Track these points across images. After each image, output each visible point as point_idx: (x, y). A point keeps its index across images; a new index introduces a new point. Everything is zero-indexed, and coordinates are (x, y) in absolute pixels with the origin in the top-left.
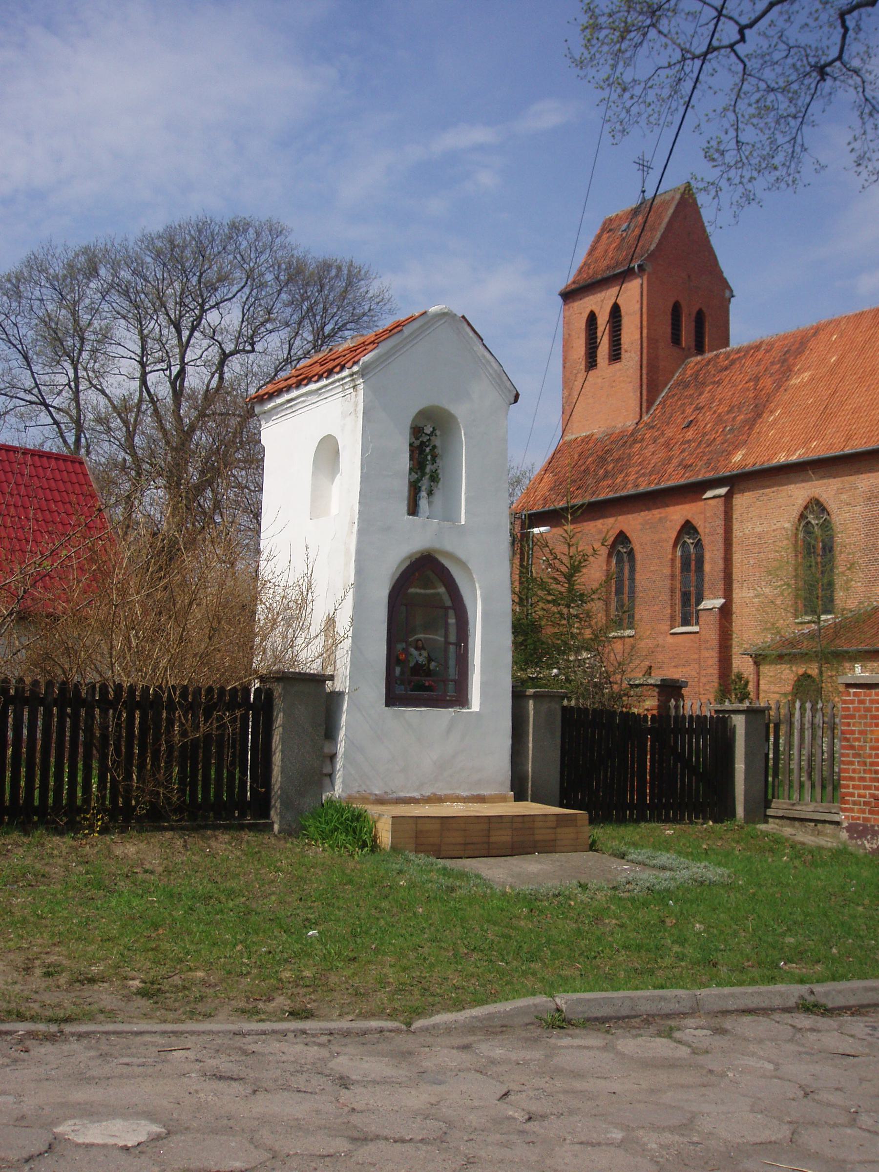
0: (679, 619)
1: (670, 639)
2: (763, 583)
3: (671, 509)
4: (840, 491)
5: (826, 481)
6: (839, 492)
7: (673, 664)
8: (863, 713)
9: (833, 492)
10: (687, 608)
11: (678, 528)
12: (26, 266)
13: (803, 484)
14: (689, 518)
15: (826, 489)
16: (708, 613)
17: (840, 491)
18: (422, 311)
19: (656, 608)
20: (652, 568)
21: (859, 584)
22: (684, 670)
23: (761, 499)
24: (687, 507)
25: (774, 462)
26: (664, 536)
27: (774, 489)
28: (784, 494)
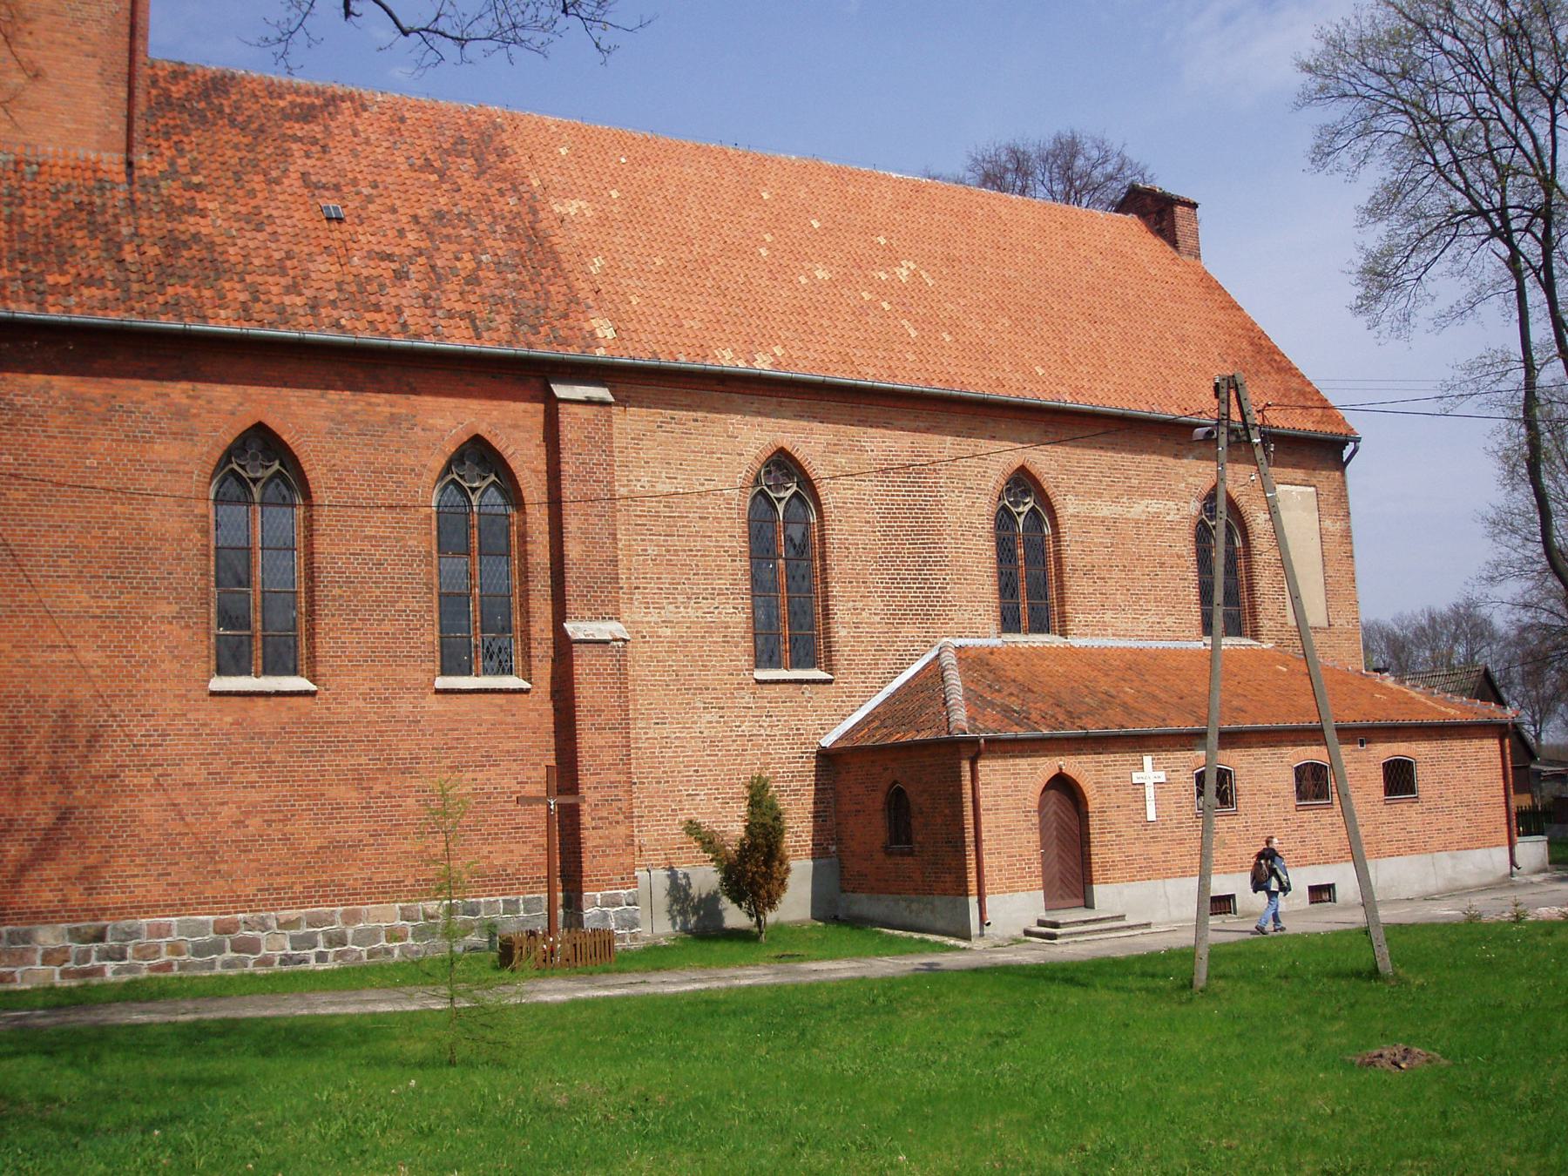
0: (1218, 623)
1: (434, 704)
2: (680, 598)
3: (427, 402)
4: (831, 448)
5: (803, 423)
6: (832, 449)
7: (448, 762)
8: (383, 943)
9: (820, 448)
10: (474, 631)
11: (451, 449)
12: (1324, 166)
13: (764, 420)
14: (482, 430)
15: (811, 441)
16: (598, 649)
17: (831, 448)
18: (1193, 199)
19: (387, 627)
20: (369, 531)
21: (877, 619)
22: (480, 776)
23: (667, 427)
24: (475, 405)
25: (710, 364)
26: (409, 461)
27: (700, 415)
28: (717, 429)
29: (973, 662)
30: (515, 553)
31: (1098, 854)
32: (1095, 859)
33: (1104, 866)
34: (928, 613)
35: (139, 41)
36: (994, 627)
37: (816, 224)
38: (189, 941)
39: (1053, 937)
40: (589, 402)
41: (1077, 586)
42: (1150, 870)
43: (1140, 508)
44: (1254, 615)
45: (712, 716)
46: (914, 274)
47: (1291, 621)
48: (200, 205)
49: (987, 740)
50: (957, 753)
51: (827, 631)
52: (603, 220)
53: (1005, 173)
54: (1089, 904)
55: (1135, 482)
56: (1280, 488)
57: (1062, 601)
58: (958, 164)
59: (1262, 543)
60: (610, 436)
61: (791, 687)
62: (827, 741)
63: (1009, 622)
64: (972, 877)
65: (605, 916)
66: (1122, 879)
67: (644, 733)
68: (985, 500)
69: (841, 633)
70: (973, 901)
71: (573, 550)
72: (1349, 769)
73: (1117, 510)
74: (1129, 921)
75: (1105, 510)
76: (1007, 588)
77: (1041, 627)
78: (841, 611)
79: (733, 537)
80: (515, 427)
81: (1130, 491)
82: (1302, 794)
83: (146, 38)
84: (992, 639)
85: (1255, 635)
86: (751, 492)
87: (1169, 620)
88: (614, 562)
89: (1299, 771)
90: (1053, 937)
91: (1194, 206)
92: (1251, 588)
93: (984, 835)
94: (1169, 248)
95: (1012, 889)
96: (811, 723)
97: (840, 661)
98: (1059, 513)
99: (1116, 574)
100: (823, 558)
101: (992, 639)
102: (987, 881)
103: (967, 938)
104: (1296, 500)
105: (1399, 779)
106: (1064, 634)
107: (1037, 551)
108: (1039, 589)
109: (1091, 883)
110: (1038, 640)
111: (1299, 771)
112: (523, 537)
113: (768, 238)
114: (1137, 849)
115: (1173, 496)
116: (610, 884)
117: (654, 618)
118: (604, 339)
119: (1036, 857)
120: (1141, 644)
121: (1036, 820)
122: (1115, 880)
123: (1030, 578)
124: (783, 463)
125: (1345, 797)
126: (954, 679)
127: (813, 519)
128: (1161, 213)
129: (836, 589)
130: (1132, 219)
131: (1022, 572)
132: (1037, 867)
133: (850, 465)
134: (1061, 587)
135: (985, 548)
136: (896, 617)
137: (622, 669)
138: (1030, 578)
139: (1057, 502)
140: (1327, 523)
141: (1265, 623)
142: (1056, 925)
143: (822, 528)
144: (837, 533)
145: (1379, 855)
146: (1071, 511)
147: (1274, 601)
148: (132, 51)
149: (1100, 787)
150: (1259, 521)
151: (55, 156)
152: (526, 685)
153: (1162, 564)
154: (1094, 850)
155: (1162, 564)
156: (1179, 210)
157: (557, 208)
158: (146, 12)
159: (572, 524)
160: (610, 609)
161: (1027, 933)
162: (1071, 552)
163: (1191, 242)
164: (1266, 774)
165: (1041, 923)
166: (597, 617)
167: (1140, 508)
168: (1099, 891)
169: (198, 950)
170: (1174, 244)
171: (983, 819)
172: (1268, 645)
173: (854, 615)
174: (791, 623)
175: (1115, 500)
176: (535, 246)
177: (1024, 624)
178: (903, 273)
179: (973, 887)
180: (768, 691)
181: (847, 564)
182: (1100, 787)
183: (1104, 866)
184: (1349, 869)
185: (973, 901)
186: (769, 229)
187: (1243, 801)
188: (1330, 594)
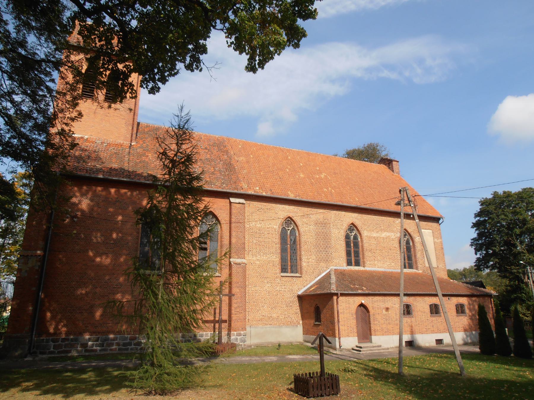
29: (341, 274)
30: (219, 241)
31: (374, 327)
32: (372, 328)
33: (375, 330)
34: (327, 260)
35: (135, 116)
36: (345, 264)
37: (301, 164)
38: (122, 342)
39: (360, 351)
40: (239, 203)
41: (367, 254)
42: (388, 332)
43: (384, 234)
44: (416, 263)
45: (269, 285)
46: (325, 176)
47: (427, 265)
48: (147, 154)
49: (341, 294)
50: (329, 297)
51: (301, 263)
52: (248, 162)
53: (353, 155)
54: (371, 342)
55: (382, 228)
56: (423, 230)
57: (363, 259)
58: (342, 152)
59: (418, 246)
60: (245, 212)
61: (290, 278)
62: (300, 293)
63: (349, 263)
64: (337, 332)
65: (237, 339)
66: (380, 335)
67: (250, 289)
68: (342, 231)
69: (304, 264)
70: (337, 339)
71: (234, 240)
72: (446, 306)
73: (378, 235)
74: (382, 347)
75: (375, 235)
76: (348, 254)
77: (357, 264)
78: (304, 258)
79: (277, 239)
80: (221, 209)
81: (381, 230)
82: (431, 313)
83: (137, 116)
84: (344, 267)
85: (417, 269)
86: (281, 227)
87: (393, 264)
88: (244, 244)
89: (431, 306)
90: (360, 351)
91: (398, 162)
92: (415, 256)
93: (340, 320)
94: (391, 172)
95: (348, 336)
96: (295, 288)
97: (304, 272)
98: (362, 235)
99: (378, 251)
100: (300, 245)
101: (344, 267)
102: (341, 333)
103: (335, 349)
104: (427, 233)
105: (435, 310)
106: (364, 267)
107: (356, 245)
108: (357, 254)
109: (371, 335)
110: (357, 268)
111: (431, 306)
112: (221, 237)
113: (289, 167)
114: (384, 326)
115: (393, 232)
116: (239, 330)
117: (254, 259)
118: (245, 188)
119: (355, 327)
120: (385, 270)
121: (355, 316)
122: (378, 335)
123: (354, 250)
124: (289, 220)
125: (445, 313)
126: (333, 277)
127: (297, 235)
128: (389, 164)
129: (303, 253)
130: (265, 67)
131: (352, 251)
132: (355, 330)
133: (307, 221)
134: (363, 254)
135: (343, 244)
136: (319, 261)
137: (245, 271)
138: (354, 250)
139: (362, 232)
140: (436, 240)
141: (420, 266)
142: (361, 347)
143: (299, 237)
144: (303, 239)
145: (456, 331)
146: (365, 234)
147: (422, 260)
148: (134, 119)
149: (373, 308)
150: (417, 239)
151: (112, 141)
152: (220, 275)
153: (390, 249)
154: (372, 326)
155: (390, 249)
156: (394, 163)
157: (236, 159)
158: (138, 109)
159: (234, 234)
160: (242, 256)
161: (353, 349)
162: (366, 245)
163: (397, 171)
164: (420, 305)
165: (357, 347)
166: (239, 258)
167: (384, 234)
168: (373, 338)
169: (124, 345)
170: (393, 171)
171: (340, 316)
172: (420, 272)
173: (307, 259)
174: (290, 262)
175: (377, 232)
176: (229, 167)
177: (353, 263)
178: (323, 176)
179: (337, 335)
180: (284, 279)
181: (306, 246)
182: (373, 308)
183: (375, 330)
184: (447, 335)
185: (337, 339)
186: (290, 165)
187: (414, 313)
188: (437, 259)
